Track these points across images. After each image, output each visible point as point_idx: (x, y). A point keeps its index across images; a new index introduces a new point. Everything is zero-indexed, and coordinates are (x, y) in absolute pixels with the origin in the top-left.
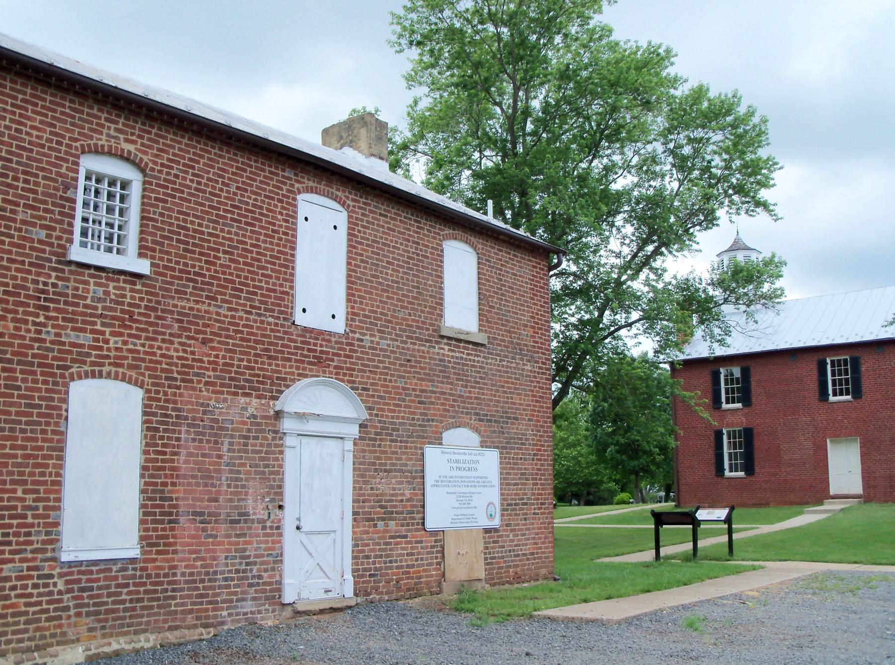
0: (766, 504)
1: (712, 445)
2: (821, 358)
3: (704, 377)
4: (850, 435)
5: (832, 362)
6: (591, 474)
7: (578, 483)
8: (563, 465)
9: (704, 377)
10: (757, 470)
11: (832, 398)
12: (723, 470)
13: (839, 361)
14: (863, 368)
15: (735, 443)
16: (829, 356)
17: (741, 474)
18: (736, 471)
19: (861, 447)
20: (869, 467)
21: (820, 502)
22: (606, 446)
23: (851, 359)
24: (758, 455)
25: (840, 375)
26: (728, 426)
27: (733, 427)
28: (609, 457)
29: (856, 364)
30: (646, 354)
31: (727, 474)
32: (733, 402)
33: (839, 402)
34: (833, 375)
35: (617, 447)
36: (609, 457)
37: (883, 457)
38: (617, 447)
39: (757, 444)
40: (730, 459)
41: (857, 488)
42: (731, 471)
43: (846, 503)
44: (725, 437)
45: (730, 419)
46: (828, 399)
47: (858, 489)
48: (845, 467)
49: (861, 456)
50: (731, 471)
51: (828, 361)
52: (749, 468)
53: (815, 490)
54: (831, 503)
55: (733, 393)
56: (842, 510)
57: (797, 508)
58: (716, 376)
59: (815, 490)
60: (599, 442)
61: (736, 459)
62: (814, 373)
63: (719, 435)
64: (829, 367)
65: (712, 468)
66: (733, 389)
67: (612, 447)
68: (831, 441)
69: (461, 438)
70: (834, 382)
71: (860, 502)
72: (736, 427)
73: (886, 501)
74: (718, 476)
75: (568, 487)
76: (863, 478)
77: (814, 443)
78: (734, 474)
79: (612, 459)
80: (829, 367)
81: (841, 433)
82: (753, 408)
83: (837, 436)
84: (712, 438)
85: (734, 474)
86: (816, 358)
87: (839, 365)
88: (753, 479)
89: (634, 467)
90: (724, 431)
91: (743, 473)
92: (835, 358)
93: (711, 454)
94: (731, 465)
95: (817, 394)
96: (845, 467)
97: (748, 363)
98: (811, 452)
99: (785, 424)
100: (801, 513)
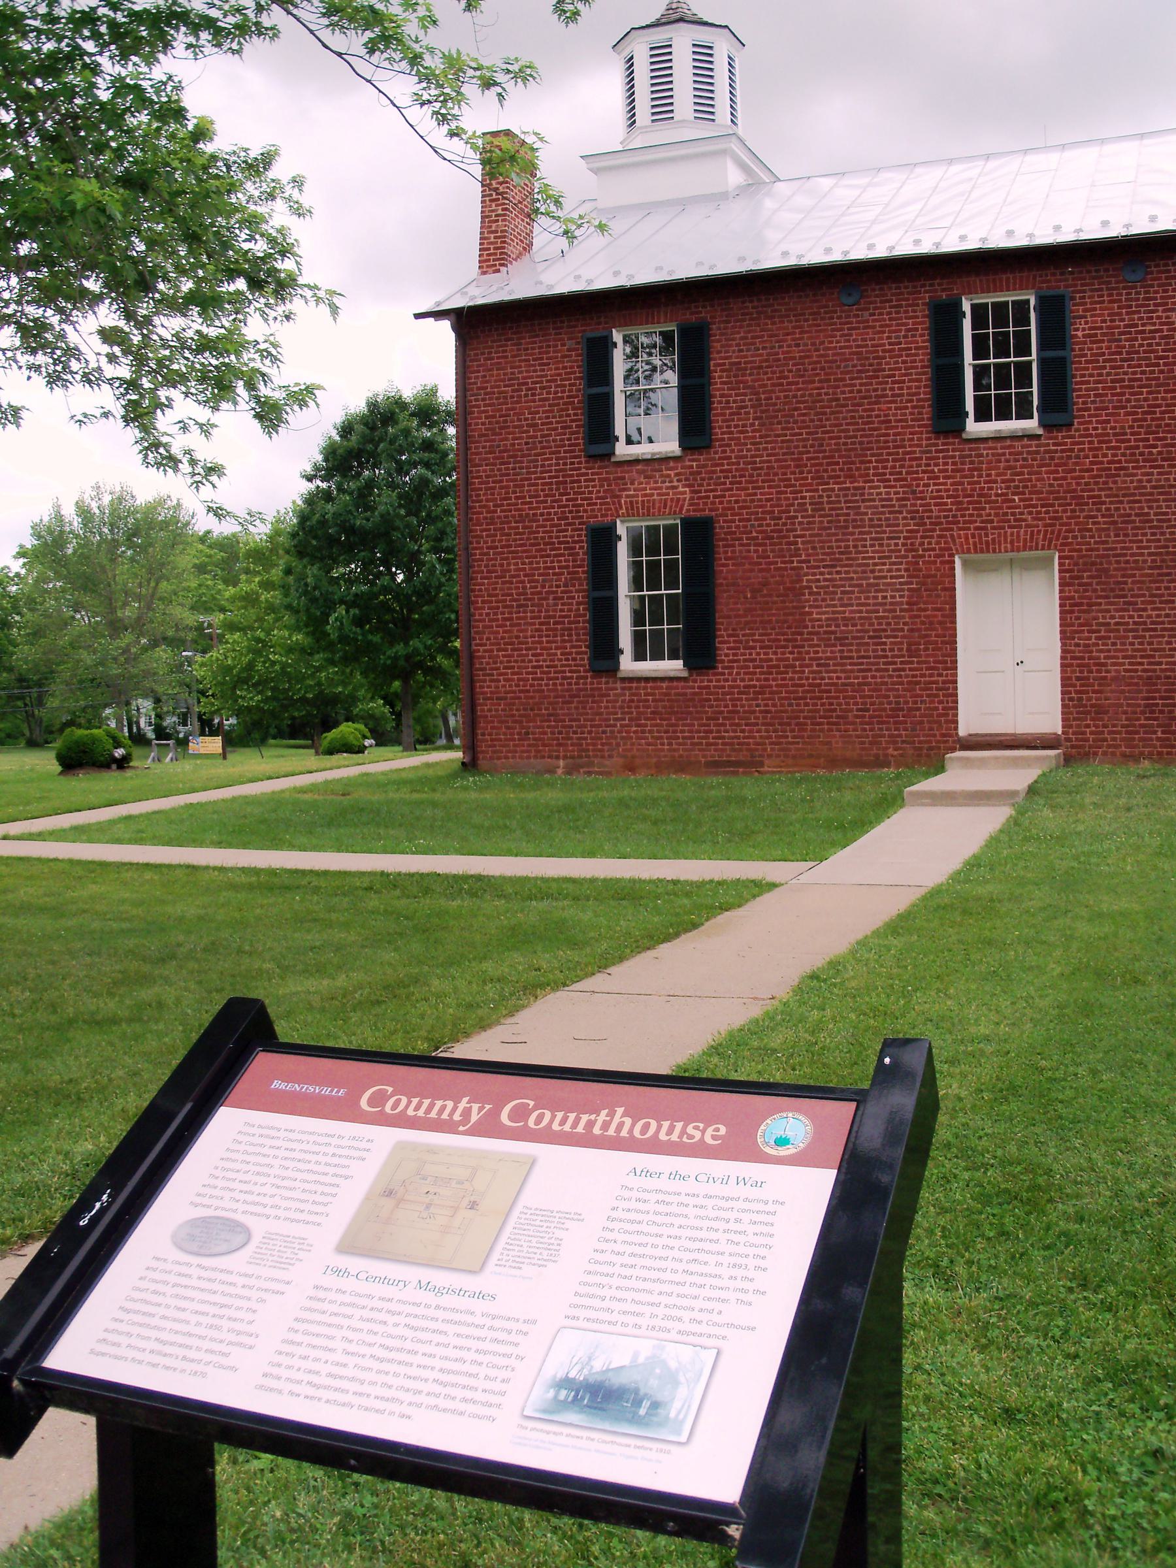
1: (582, 573)
5: (979, 312)
6: (331, 681)
7: (303, 700)
8: (274, 663)
10: (724, 651)
11: (974, 428)
12: (614, 652)
13: (1000, 308)
14: (1079, 331)
15: (654, 566)
16: (970, 292)
17: (673, 666)
18: (657, 656)
22: (330, 605)
23: (1041, 300)
26: (633, 511)
27: (648, 514)
28: (334, 636)
29: (1054, 316)
30: (434, 392)
31: (628, 664)
33: (998, 439)
34: (980, 350)
35: (354, 611)
36: (334, 636)
38: (354, 611)
39: (725, 568)
42: (639, 656)
44: (622, 549)
45: (638, 489)
46: (616, 667)
47: (1050, 721)
48: (1009, 647)
49: (1062, 612)
50: (639, 656)
51: (966, 306)
52: (699, 651)
53: (914, 728)
57: (863, 785)
58: (945, 322)
59: (914, 728)
60: (313, 600)
61: (656, 620)
62: (922, 340)
63: (602, 542)
64: (967, 324)
67: (341, 610)
68: (965, 563)
70: (980, 373)
72: (661, 515)
74: (597, 672)
75: (285, 708)
76: (1066, 682)
77: (913, 570)
78: (649, 667)
79: (344, 639)
80: (967, 324)
82: (716, 453)
83: (987, 548)
84: (582, 551)
85: (649, 667)
87: (1000, 321)
88: (703, 680)
89: (396, 658)
90: (621, 530)
91: (678, 664)
92: (989, 299)
93: (576, 603)
94: (639, 638)
95: (927, 412)
96: (1009, 647)
97: (703, 312)
98: (901, 598)
99: (818, 506)
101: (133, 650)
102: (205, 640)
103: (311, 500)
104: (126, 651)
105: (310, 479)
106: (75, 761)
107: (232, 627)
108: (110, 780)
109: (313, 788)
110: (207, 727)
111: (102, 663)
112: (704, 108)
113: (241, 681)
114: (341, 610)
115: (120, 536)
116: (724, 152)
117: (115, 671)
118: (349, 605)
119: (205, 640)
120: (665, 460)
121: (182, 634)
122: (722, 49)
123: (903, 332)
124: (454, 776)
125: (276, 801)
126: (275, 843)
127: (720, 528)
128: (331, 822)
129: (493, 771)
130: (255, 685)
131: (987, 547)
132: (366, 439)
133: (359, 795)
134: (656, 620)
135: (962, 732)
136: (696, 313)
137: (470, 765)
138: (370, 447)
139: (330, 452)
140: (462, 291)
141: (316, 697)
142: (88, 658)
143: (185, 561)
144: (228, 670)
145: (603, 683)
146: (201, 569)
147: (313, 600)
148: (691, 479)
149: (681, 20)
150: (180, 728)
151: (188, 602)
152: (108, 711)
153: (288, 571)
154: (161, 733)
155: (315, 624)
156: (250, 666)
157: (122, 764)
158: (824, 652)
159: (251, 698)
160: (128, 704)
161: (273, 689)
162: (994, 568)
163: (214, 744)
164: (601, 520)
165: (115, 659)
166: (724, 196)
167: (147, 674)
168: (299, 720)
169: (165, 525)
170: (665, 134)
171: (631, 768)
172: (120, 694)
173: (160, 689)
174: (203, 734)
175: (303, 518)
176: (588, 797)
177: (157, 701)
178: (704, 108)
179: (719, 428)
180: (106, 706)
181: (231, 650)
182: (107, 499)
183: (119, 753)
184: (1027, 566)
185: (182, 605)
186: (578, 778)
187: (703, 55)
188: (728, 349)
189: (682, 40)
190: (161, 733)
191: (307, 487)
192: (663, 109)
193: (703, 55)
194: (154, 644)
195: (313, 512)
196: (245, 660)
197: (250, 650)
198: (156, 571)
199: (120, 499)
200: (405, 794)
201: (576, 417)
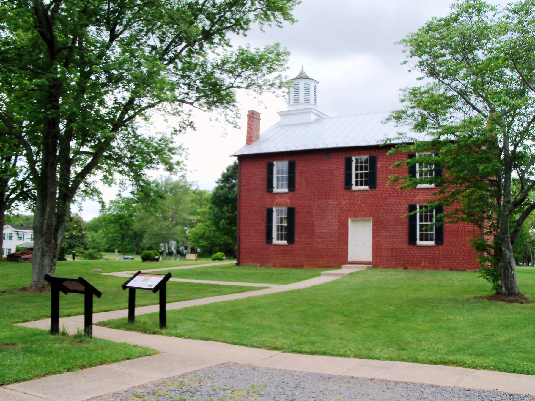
0: (301, 266)
1: (265, 219)
2: (348, 156)
3: (260, 170)
4: (365, 216)
9: (260, 170)
10: (296, 239)
14: (379, 165)
16: (354, 155)
17: (285, 242)
18: (282, 239)
19: (373, 226)
20: (378, 241)
21: (339, 267)
22: (221, 219)
24: (298, 229)
25: (361, 170)
29: (373, 161)
32: (361, 185)
33: (359, 191)
35: (227, 221)
36: (222, 227)
37: (388, 234)
38: (227, 221)
39: (298, 219)
40: (421, 230)
41: (367, 255)
43: (358, 268)
45: (278, 200)
46: (350, 188)
48: (360, 240)
54: (347, 268)
55: (361, 177)
56: (351, 274)
58: (348, 162)
59: (337, 256)
60: (216, 217)
61: (282, 231)
63: (270, 212)
65: (264, 237)
66: (362, 174)
67: (223, 221)
69: (74, 209)
71: (369, 268)
73: (387, 267)
76: (373, 249)
81: (358, 214)
82: (296, 192)
84: (265, 214)
86: (344, 156)
93: (263, 227)
94: (421, 235)
95: (344, 184)
96: (360, 240)
97: (374, 153)
98: (336, 228)
99: (318, 206)
100: (319, 275)
101: (170, 226)
102: (192, 225)
103: (217, 189)
104: (168, 226)
105: (217, 183)
106: (146, 259)
107: (199, 221)
108: (154, 264)
109: (200, 268)
110: (193, 251)
111: (160, 230)
112: (307, 100)
113: (201, 238)
114: (223, 221)
115: (168, 189)
116: (310, 112)
117: (164, 232)
118: (226, 219)
119: (192, 225)
120: (285, 193)
121: (185, 222)
122: (312, 85)
123: (339, 164)
124: (234, 266)
125: (189, 270)
126: (184, 277)
127: (296, 210)
128: (198, 274)
129: (243, 265)
130: (206, 239)
131: (356, 216)
132: (233, 173)
133: (210, 270)
134: (282, 231)
135: (350, 260)
136: (293, 157)
137: (238, 264)
138: (234, 175)
139: (224, 175)
140: (241, 150)
141: (224, 244)
142: (156, 228)
143: (188, 199)
144: (197, 234)
145: (269, 246)
146: (193, 201)
147: (216, 217)
148: (290, 198)
149: (301, 78)
150: (184, 251)
151: (188, 212)
152: (162, 244)
153: (210, 208)
154: (178, 252)
155: (216, 224)
156: (204, 233)
157: (157, 260)
158: (319, 240)
159: (204, 243)
160: (168, 242)
161: (211, 241)
162: (359, 221)
163: (193, 257)
164: (269, 207)
165: (164, 229)
166: (310, 123)
167: (174, 234)
168: (207, 253)
169: (182, 187)
170: (297, 107)
171: (274, 266)
172: (166, 240)
173: (178, 238)
174: (191, 253)
175: (215, 194)
176: (256, 272)
177: (178, 242)
178: (307, 100)
179: (297, 186)
180: (162, 243)
181: (199, 228)
182: (164, 179)
183: (157, 257)
184: (367, 221)
185: (186, 213)
186: (263, 268)
187: (307, 86)
188: (299, 168)
189: (302, 83)
190: (178, 252)
191: (216, 185)
192: (296, 99)
193: (307, 86)
194: (177, 224)
195: (217, 192)
196: (203, 231)
197: (204, 229)
198: (178, 202)
199: (168, 179)
200: (219, 270)
201: (265, 182)
